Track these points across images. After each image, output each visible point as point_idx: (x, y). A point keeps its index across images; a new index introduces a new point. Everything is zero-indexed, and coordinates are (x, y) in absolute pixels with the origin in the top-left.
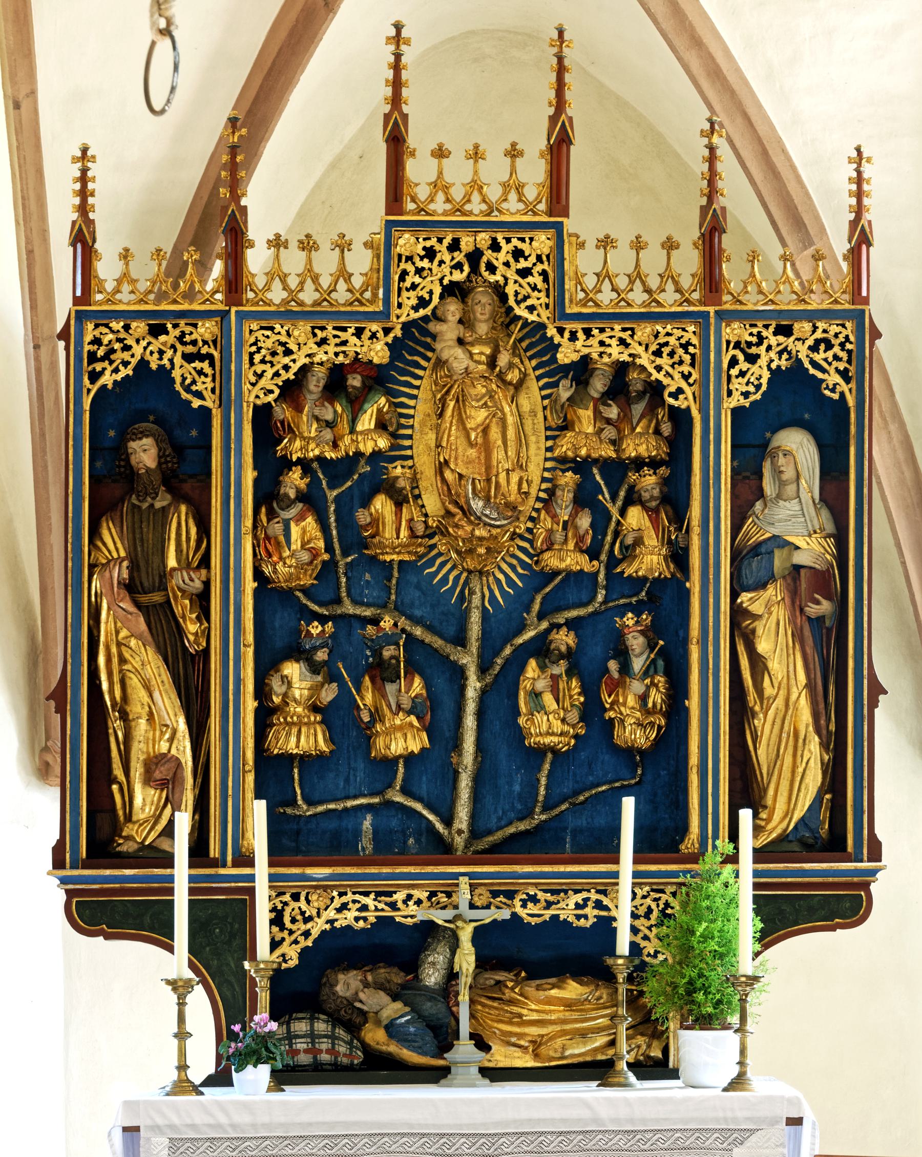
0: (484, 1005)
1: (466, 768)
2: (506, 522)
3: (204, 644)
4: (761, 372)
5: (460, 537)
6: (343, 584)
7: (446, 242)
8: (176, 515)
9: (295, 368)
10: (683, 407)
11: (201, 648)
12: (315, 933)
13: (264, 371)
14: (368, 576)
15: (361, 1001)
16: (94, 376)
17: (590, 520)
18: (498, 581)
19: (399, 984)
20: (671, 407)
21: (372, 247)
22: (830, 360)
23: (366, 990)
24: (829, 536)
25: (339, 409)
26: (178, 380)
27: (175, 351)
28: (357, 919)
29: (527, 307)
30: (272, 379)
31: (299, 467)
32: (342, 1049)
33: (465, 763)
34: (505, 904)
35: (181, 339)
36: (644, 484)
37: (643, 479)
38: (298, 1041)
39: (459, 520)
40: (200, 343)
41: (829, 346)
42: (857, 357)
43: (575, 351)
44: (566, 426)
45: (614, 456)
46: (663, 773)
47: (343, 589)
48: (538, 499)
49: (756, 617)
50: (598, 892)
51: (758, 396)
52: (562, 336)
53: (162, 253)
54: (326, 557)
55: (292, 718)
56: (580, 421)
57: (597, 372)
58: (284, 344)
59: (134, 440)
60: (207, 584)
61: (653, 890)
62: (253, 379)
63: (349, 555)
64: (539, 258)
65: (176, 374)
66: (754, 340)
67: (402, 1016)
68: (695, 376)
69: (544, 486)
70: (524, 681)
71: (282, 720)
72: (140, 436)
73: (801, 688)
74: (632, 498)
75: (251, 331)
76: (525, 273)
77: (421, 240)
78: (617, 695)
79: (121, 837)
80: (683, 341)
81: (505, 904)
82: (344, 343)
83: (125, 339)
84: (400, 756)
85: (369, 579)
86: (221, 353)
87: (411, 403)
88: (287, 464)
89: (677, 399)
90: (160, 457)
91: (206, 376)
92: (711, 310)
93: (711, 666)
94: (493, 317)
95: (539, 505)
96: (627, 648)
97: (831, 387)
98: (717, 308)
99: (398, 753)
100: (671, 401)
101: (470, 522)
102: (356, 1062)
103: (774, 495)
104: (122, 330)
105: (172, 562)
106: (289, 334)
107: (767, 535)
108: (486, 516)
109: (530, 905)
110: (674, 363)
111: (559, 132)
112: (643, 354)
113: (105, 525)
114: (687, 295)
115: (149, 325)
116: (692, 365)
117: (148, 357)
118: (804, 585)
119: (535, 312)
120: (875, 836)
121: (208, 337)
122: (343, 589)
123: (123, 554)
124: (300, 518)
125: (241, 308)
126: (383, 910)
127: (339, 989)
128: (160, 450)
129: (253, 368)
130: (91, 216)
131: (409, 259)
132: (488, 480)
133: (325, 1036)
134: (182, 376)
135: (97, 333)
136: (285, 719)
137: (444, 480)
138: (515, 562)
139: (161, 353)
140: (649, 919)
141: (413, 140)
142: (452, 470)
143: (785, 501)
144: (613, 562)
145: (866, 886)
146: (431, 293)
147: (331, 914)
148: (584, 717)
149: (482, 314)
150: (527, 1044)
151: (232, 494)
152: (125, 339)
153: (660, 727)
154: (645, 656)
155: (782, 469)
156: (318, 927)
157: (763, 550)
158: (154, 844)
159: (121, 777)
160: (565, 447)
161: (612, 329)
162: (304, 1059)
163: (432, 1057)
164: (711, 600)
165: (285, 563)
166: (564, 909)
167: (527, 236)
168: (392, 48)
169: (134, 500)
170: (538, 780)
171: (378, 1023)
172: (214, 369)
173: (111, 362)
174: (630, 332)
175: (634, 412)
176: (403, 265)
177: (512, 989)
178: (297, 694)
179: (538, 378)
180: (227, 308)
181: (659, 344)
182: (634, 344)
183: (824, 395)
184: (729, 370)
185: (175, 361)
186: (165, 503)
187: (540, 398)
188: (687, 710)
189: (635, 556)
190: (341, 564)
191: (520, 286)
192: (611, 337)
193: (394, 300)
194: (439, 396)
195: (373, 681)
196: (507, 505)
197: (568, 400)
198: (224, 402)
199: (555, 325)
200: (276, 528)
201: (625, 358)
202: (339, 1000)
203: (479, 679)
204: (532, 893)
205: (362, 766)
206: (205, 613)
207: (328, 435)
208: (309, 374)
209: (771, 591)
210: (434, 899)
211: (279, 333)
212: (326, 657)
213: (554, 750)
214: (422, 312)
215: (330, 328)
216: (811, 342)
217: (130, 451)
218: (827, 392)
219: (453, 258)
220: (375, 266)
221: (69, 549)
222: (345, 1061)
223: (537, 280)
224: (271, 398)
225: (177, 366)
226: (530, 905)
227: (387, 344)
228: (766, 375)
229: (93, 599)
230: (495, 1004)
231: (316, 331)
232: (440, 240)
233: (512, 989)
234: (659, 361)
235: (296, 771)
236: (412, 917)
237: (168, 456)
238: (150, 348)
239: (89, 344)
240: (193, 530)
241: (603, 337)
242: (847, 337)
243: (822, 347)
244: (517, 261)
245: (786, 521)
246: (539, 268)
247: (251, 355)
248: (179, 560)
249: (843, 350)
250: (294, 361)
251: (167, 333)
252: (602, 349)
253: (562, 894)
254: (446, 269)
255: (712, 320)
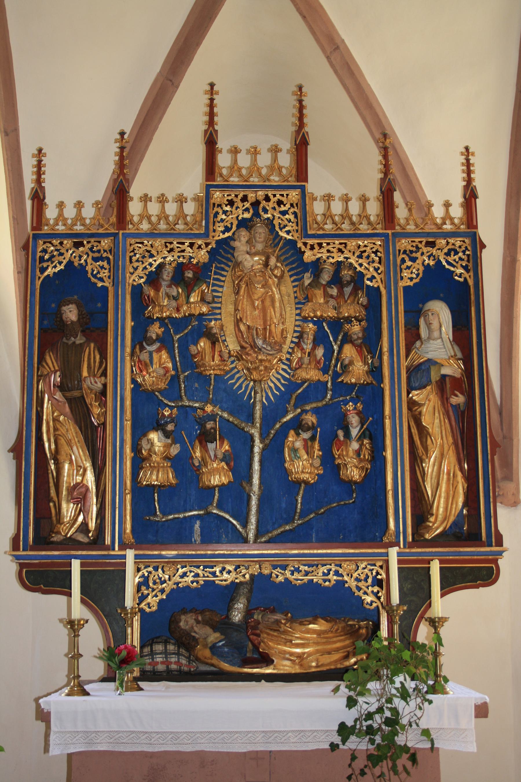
0: (268, 634)
1: (255, 493)
2: (275, 352)
3: (103, 420)
4: (418, 268)
5: (249, 360)
6: (183, 388)
7: (240, 197)
8: (88, 348)
9: (155, 264)
10: (376, 286)
11: (101, 422)
12: (168, 590)
13: (138, 266)
14: (196, 385)
15: (195, 632)
16: (43, 270)
17: (323, 351)
18: (270, 388)
19: (218, 622)
20: (368, 286)
21: (198, 200)
22: (457, 260)
23: (198, 625)
24: (460, 359)
25: (180, 290)
26: (90, 271)
27: (88, 256)
28: (192, 582)
29: (286, 231)
30: (143, 270)
31: (158, 322)
32: (184, 661)
33: (254, 490)
34: (280, 573)
35: (91, 249)
36: (353, 331)
37: (353, 328)
38: (157, 656)
39: (249, 351)
40: (102, 252)
41: (456, 253)
42: (473, 258)
43: (314, 255)
44: (308, 299)
45: (336, 315)
46: (367, 496)
47: (183, 391)
48: (292, 342)
49: (420, 405)
50: (336, 565)
51: (417, 280)
52: (306, 247)
53: (81, 204)
54: (173, 373)
55: (154, 464)
56: (316, 297)
57: (325, 270)
58: (149, 251)
59: (65, 306)
60: (105, 385)
61: (369, 564)
62: (132, 270)
63: (185, 372)
64: (292, 205)
65: (89, 268)
66: (414, 249)
67: (220, 641)
68: (382, 269)
69: (296, 335)
70: (287, 442)
71: (148, 465)
72: (68, 303)
73: (450, 444)
74: (347, 339)
75: (131, 245)
76: (284, 213)
77: (226, 196)
78: (342, 451)
79: (53, 532)
80: (374, 250)
81: (280, 573)
82: (183, 251)
83: (60, 249)
84: (217, 486)
85: (198, 386)
86: (114, 256)
87: (220, 290)
88: (151, 320)
89: (372, 282)
90: (79, 315)
91: (106, 269)
92: (389, 232)
93: (398, 431)
94: (266, 241)
95: (293, 345)
96: (348, 423)
97: (458, 275)
98: (393, 231)
99: (216, 484)
100: (368, 283)
101: (255, 352)
102: (192, 669)
103: (426, 338)
104: (59, 245)
105: (85, 373)
106: (152, 246)
107: (425, 359)
108: (264, 348)
109: (296, 574)
110: (369, 262)
111: (301, 139)
112: (352, 257)
113: (47, 354)
114: (375, 226)
115: (74, 242)
116: (380, 263)
117: (73, 259)
118: (448, 386)
119: (291, 234)
120: (498, 531)
121: (106, 247)
122: (183, 391)
123: (57, 368)
124: (159, 350)
125: (125, 231)
126: (208, 577)
127: (182, 624)
128: (79, 311)
129: (132, 264)
130: (43, 185)
131: (219, 206)
132: (265, 329)
133: (173, 654)
134: (92, 269)
135: (45, 246)
136: (150, 464)
137: (239, 330)
138: (279, 377)
139: (80, 257)
140: (367, 582)
141: (220, 145)
142: (244, 324)
143: (434, 340)
144: (336, 375)
145: (495, 562)
146: (232, 224)
147: (177, 579)
148: (323, 463)
149: (259, 238)
150: (295, 659)
151: (119, 333)
152: (60, 249)
153: (367, 469)
154: (358, 428)
155: (431, 322)
156: (168, 587)
157: (423, 367)
158: (73, 537)
159: (55, 499)
160: (308, 311)
161: (334, 243)
162: (161, 668)
163: (239, 667)
164: (397, 393)
165: (150, 375)
166: (316, 576)
167: (285, 193)
168: (208, 96)
169: (64, 340)
170: (297, 500)
171: (205, 646)
172: (110, 265)
173: (52, 263)
174: (344, 245)
175: (345, 293)
176: (216, 209)
177: (285, 624)
178: (157, 449)
179: (291, 276)
180: (117, 232)
181: (361, 251)
182: (346, 252)
183: (455, 279)
184: (401, 266)
185: (88, 261)
186: (82, 341)
187: (292, 287)
188: (385, 458)
189: (349, 372)
190: (182, 377)
191: (282, 220)
192: (333, 248)
193: (211, 227)
194: (237, 282)
195: (201, 443)
196: (276, 343)
197: (309, 285)
198: (115, 284)
199: (302, 241)
200: (144, 356)
201: (341, 259)
202: (182, 631)
203: (261, 442)
204: (296, 566)
205: (194, 492)
206: (103, 404)
207: (174, 304)
208: (163, 270)
209: (429, 388)
210: (238, 570)
211: (146, 245)
212: (173, 428)
213: (306, 483)
214: (227, 235)
215: (175, 243)
216: (446, 250)
217: (62, 312)
218: (456, 278)
219: (244, 206)
220: (200, 210)
221: (26, 365)
222: (186, 669)
223: (291, 217)
224: (142, 280)
225: (89, 264)
226: (296, 574)
227: (207, 252)
228: (422, 269)
229: (40, 395)
230: (275, 634)
231: (167, 244)
232: (236, 196)
233: (285, 624)
234: (360, 261)
235: (156, 495)
236: (225, 580)
237: (84, 314)
238: (74, 255)
239: (40, 252)
240: (98, 357)
241: (330, 247)
242: (466, 248)
243: (452, 253)
244: (279, 206)
245: (435, 351)
246: (292, 210)
247: (131, 258)
248: (89, 372)
249: (464, 254)
250: (155, 261)
251: (83, 246)
252: (328, 254)
253: (314, 567)
254: (240, 212)
255: (390, 238)
